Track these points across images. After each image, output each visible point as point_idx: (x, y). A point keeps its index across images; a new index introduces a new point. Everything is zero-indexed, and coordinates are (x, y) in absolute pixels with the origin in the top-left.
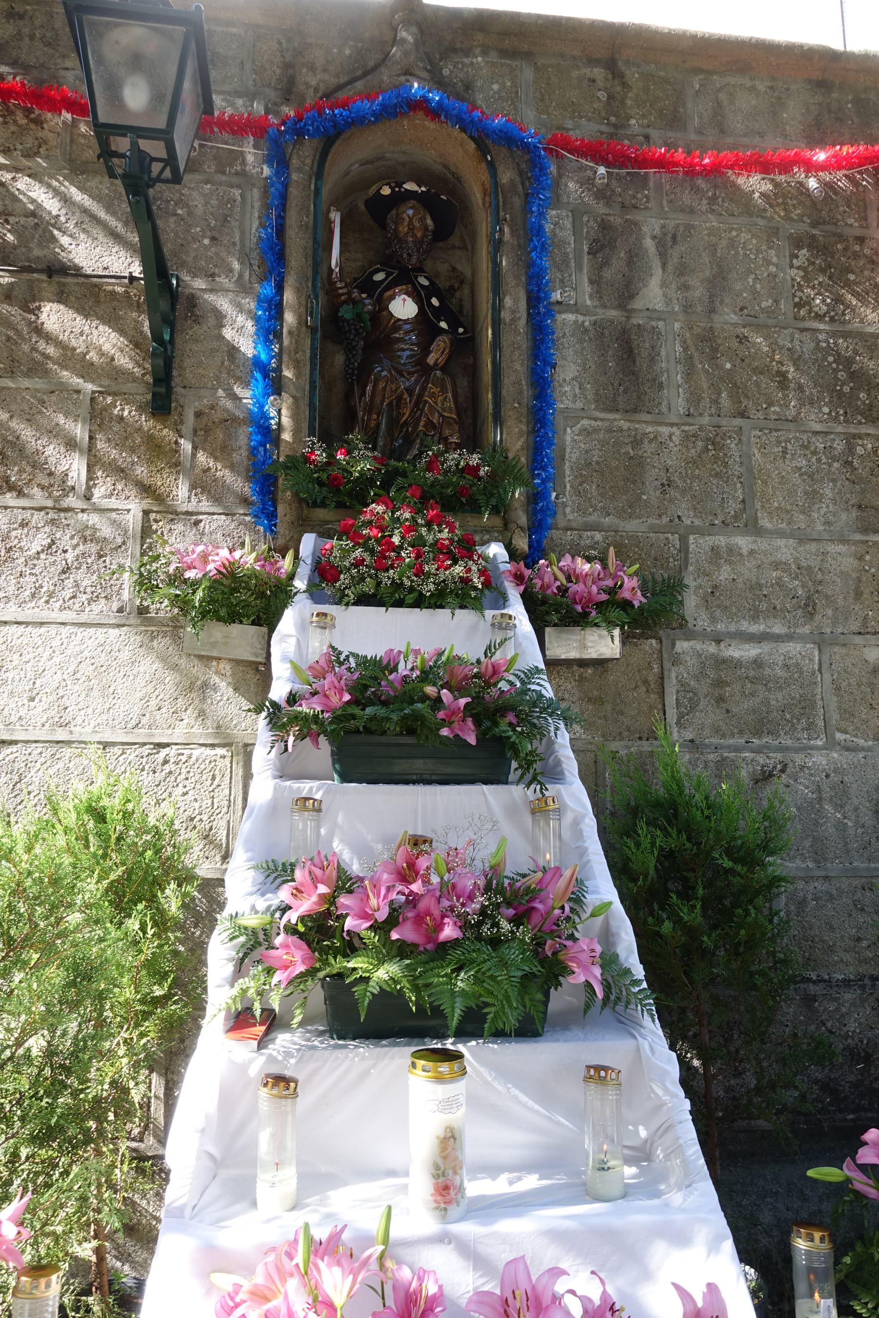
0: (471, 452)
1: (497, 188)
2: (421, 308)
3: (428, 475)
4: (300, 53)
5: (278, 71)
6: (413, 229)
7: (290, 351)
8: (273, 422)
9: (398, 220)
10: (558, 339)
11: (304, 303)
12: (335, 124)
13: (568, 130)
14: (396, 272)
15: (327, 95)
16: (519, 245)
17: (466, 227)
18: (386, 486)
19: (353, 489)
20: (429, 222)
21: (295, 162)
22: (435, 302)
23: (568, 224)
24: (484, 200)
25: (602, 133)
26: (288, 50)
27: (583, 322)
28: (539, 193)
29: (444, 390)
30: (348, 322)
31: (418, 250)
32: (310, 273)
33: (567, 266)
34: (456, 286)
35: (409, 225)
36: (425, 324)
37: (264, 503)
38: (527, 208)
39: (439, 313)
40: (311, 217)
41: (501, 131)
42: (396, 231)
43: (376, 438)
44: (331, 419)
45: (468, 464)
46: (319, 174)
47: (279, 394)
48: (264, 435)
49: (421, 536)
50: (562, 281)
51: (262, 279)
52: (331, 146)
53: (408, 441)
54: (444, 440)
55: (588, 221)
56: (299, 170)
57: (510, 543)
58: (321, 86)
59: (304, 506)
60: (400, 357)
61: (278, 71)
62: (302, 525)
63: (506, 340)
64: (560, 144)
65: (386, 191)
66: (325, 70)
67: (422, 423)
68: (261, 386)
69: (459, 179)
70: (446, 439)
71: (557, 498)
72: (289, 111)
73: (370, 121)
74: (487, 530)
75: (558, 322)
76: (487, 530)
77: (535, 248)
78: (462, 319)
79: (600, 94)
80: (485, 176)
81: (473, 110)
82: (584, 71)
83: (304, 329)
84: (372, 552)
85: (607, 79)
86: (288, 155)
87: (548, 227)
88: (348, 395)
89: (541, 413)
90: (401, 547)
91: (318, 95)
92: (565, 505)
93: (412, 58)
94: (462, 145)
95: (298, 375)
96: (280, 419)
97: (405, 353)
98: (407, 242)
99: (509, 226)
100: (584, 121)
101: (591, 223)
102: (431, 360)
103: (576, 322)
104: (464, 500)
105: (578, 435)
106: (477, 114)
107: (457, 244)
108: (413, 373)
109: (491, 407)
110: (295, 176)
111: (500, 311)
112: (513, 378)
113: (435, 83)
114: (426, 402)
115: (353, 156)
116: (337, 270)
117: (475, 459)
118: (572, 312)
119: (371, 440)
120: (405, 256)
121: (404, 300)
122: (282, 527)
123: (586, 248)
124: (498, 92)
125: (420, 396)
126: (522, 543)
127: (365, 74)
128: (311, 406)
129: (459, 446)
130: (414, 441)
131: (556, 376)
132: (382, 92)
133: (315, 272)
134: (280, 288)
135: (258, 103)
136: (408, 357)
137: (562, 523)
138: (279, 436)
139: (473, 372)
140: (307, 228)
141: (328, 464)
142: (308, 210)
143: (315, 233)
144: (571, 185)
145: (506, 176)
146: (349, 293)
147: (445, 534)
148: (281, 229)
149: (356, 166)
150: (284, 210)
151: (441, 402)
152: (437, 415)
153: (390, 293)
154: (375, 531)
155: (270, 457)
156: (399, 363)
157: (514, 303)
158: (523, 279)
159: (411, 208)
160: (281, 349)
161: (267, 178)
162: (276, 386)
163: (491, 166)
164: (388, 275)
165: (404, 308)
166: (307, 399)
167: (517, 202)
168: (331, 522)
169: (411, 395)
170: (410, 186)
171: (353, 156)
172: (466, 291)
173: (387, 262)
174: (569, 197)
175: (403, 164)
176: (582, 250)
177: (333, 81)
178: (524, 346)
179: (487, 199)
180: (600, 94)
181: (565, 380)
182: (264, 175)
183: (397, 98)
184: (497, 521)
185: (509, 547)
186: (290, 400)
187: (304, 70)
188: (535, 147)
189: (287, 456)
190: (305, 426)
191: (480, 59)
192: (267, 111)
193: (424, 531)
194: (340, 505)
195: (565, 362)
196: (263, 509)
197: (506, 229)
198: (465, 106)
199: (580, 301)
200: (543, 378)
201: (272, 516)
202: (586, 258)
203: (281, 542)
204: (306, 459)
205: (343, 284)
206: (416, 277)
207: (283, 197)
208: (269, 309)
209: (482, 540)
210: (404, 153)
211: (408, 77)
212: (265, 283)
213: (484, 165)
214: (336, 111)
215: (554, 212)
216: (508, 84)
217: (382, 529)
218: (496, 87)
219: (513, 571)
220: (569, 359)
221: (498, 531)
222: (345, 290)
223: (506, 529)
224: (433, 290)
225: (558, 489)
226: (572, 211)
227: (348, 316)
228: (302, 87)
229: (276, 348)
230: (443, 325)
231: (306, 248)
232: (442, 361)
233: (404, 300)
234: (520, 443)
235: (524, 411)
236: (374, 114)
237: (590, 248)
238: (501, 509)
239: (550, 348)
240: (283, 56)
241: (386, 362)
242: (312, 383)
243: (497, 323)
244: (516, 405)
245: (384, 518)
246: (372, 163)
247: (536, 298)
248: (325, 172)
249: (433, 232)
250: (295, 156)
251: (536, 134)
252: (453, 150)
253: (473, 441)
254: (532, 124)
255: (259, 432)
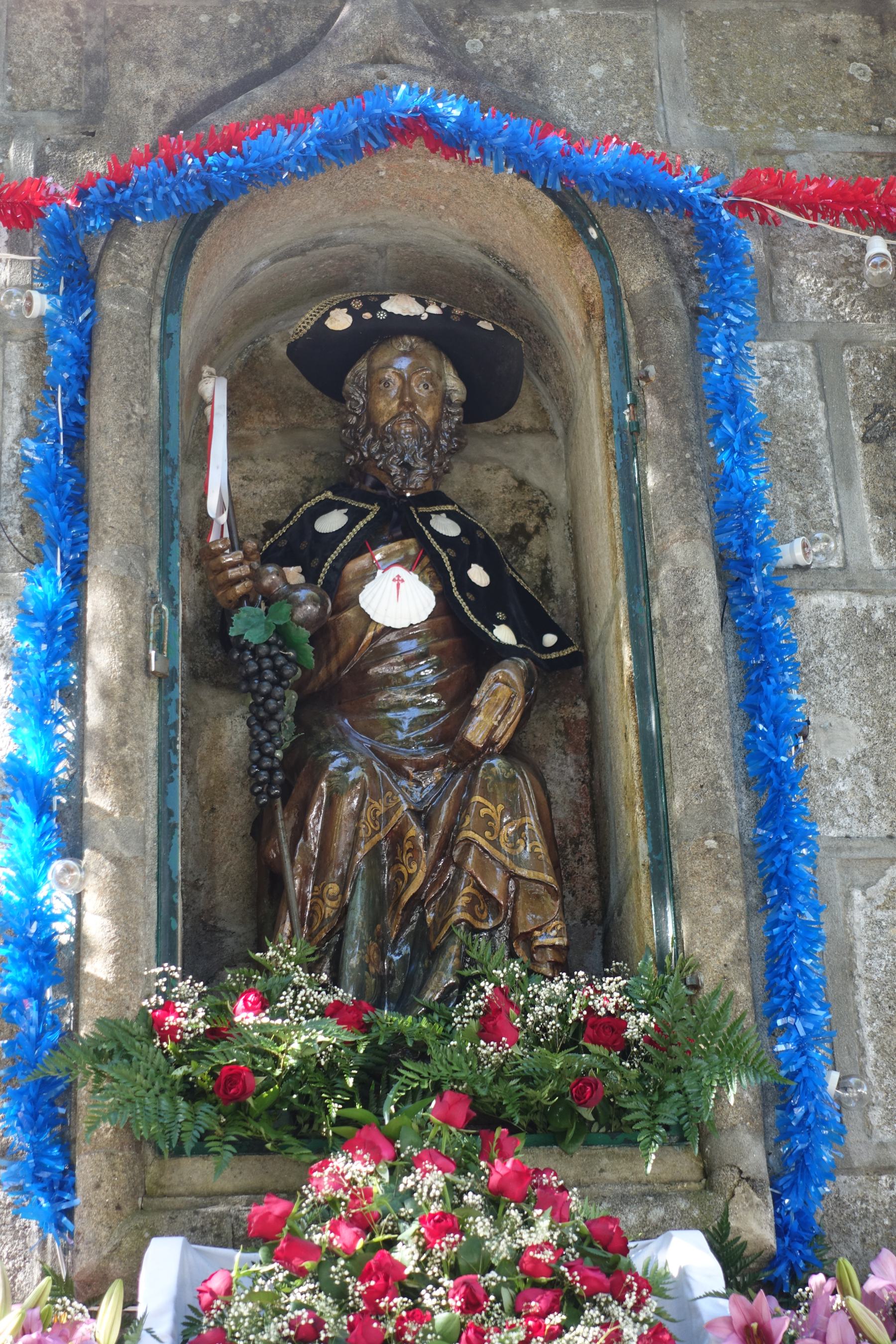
0: (599, 972)
1: (617, 301)
2: (444, 597)
3: (486, 1049)
4: (121, 28)
5: (67, 73)
6: (412, 405)
7: (104, 741)
8: (58, 926)
9: (372, 386)
10: (808, 658)
11: (138, 614)
12: (208, 188)
13: (784, 154)
14: (376, 508)
15: (185, 120)
16: (686, 437)
17: (546, 380)
18: (374, 1081)
19: (282, 1099)
20: (453, 383)
21: (110, 278)
22: (478, 575)
23: (805, 372)
24: (587, 328)
25: (868, 155)
26: (90, 26)
27: (869, 611)
28: (724, 310)
29: (515, 809)
30: (254, 651)
31: (428, 455)
32: (153, 538)
33: (814, 474)
34: (531, 526)
35: (401, 396)
36: (460, 644)
37: (38, 1153)
38: (698, 347)
39: (489, 603)
40: (154, 403)
41: (618, 175)
42: (368, 411)
43: (340, 946)
44: (218, 920)
45: (591, 1011)
46: (172, 301)
47: (76, 853)
48: (38, 965)
49: (479, 1241)
50: (804, 511)
51: (35, 558)
52: (199, 234)
53: (426, 950)
54: (521, 942)
55: (856, 362)
56: (123, 295)
57: (724, 1225)
58: (173, 97)
59: (149, 1153)
60: (394, 725)
61: (67, 73)
62: (148, 1210)
63: (671, 674)
64: (771, 192)
65: (340, 321)
66: (180, 63)
67: (461, 901)
68: (29, 830)
69: (521, 278)
70: (528, 938)
71: (842, 1085)
72: (95, 163)
73: (295, 174)
74: (655, 1193)
75: (803, 616)
76: (655, 1193)
77: (727, 442)
78: (551, 608)
79: (852, 69)
80: (586, 273)
81: (544, 134)
82: (808, 21)
83: (140, 681)
84: (340, 1295)
85: (867, 35)
86: (93, 261)
87: (755, 387)
88: (260, 828)
89: (779, 859)
90: (422, 1278)
91: (167, 119)
92: (865, 1103)
93: (390, 26)
94: (524, 207)
95: (127, 803)
96: (79, 917)
97: (411, 701)
98: (397, 437)
99: (655, 392)
100: (820, 133)
101: (865, 367)
102: (476, 732)
103: (849, 613)
104: (587, 1114)
105: (885, 907)
106: (555, 141)
107: (526, 422)
108: (431, 765)
109: (643, 847)
110: (110, 305)
111: (648, 601)
112: (697, 773)
113: (449, 76)
114: (469, 842)
115: (248, 249)
116: (223, 519)
117: (608, 995)
118: (836, 588)
119: (327, 956)
120: (395, 470)
121: (399, 580)
122: (89, 1221)
123: (857, 429)
124: (604, 82)
125: (453, 827)
126: (756, 1226)
127: (280, 66)
128: (164, 878)
129: (564, 963)
130: (442, 949)
131: (811, 758)
132: (318, 108)
133: (167, 535)
134: (76, 578)
135: (20, 148)
136: (415, 723)
137: (863, 1156)
138: (76, 967)
139: (590, 744)
140: (143, 431)
141: (214, 1035)
142: (146, 387)
143: (164, 439)
144: (804, 280)
145: (640, 274)
146: (255, 576)
147: (542, 1229)
148: (76, 438)
149: (265, 262)
150: (84, 391)
151: (510, 839)
152: (500, 875)
153: (362, 562)
154: (347, 1233)
155: (55, 1024)
156: (393, 740)
157: (686, 557)
158: (704, 518)
159: (405, 354)
160: (81, 730)
161: (42, 319)
162: (69, 834)
163: (601, 250)
164: (355, 516)
165: (397, 598)
166: (151, 862)
167: (673, 335)
168: (223, 1195)
169: (427, 825)
170: (400, 305)
171: (248, 249)
172: (557, 533)
173: (349, 483)
174: (800, 307)
175: (381, 250)
176: (846, 433)
177: (197, 84)
178: (720, 689)
179: (596, 327)
180: (852, 69)
181: (834, 764)
182: (36, 312)
183: (357, 117)
184: (684, 1164)
185: (724, 1246)
186: (108, 869)
187: (131, 66)
188: (705, 203)
189: (101, 1023)
190: (147, 933)
191: (554, 12)
192: (42, 168)
193: (482, 1226)
194: (250, 1147)
195: (830, 718)
196: (39, 1167)
197: (651, 402)
198: (524, 127)
199: (855, 560)
200: (775, 765)
201: (60, 1186)
202: (859, 452)
203: (86, 1261)
204: (153, 1026)
205: (239, 555)
206: (426, 518)
207: (83, 363)
208: (49, 637)
209: (644, 1222)
210: (382, 225)
211: (385, 69)
212: (38, 570)
213: (581, 249)
214: (210, 160)
215: (768, 347)
216: (628, 61)
217: (364, 1224)
218: (597, 70)
219: (739, 1320)
220: (842, 707)
221: (687, 1195)
222: (244, 570)
223: (709, 1187)
224: (473, 545)
225: (844, 1059)
226: (813, 342)
227: (254, 636)
228: (126, 105)
229: (67, 731)
230: (504, 634)
231: (141, 479)
232: (503, 734)
233: (399, 580)
234: (729, 946)
235: (734, 857)
236: (303, 157)
237: (867, 428)
238: (691, 1131)
239: (787, 687)
240: (79, 40)
241: (360, 742)
242: (165, 815)
243: (643, 632)
244: (711, 843)
245: (368, 1194)
246: (303, 252)
247: (741, 566)
248: (187, 294)
249: (464, 405)
250: (109, 264)
251: (706, 173)
252: (502, 219)
253: (599, 939)
254: (692, 145)
255: (26, 959)
